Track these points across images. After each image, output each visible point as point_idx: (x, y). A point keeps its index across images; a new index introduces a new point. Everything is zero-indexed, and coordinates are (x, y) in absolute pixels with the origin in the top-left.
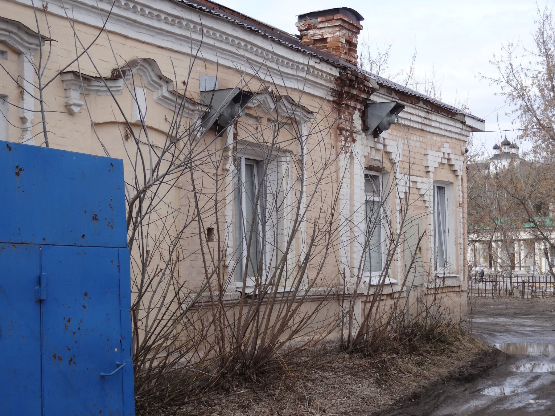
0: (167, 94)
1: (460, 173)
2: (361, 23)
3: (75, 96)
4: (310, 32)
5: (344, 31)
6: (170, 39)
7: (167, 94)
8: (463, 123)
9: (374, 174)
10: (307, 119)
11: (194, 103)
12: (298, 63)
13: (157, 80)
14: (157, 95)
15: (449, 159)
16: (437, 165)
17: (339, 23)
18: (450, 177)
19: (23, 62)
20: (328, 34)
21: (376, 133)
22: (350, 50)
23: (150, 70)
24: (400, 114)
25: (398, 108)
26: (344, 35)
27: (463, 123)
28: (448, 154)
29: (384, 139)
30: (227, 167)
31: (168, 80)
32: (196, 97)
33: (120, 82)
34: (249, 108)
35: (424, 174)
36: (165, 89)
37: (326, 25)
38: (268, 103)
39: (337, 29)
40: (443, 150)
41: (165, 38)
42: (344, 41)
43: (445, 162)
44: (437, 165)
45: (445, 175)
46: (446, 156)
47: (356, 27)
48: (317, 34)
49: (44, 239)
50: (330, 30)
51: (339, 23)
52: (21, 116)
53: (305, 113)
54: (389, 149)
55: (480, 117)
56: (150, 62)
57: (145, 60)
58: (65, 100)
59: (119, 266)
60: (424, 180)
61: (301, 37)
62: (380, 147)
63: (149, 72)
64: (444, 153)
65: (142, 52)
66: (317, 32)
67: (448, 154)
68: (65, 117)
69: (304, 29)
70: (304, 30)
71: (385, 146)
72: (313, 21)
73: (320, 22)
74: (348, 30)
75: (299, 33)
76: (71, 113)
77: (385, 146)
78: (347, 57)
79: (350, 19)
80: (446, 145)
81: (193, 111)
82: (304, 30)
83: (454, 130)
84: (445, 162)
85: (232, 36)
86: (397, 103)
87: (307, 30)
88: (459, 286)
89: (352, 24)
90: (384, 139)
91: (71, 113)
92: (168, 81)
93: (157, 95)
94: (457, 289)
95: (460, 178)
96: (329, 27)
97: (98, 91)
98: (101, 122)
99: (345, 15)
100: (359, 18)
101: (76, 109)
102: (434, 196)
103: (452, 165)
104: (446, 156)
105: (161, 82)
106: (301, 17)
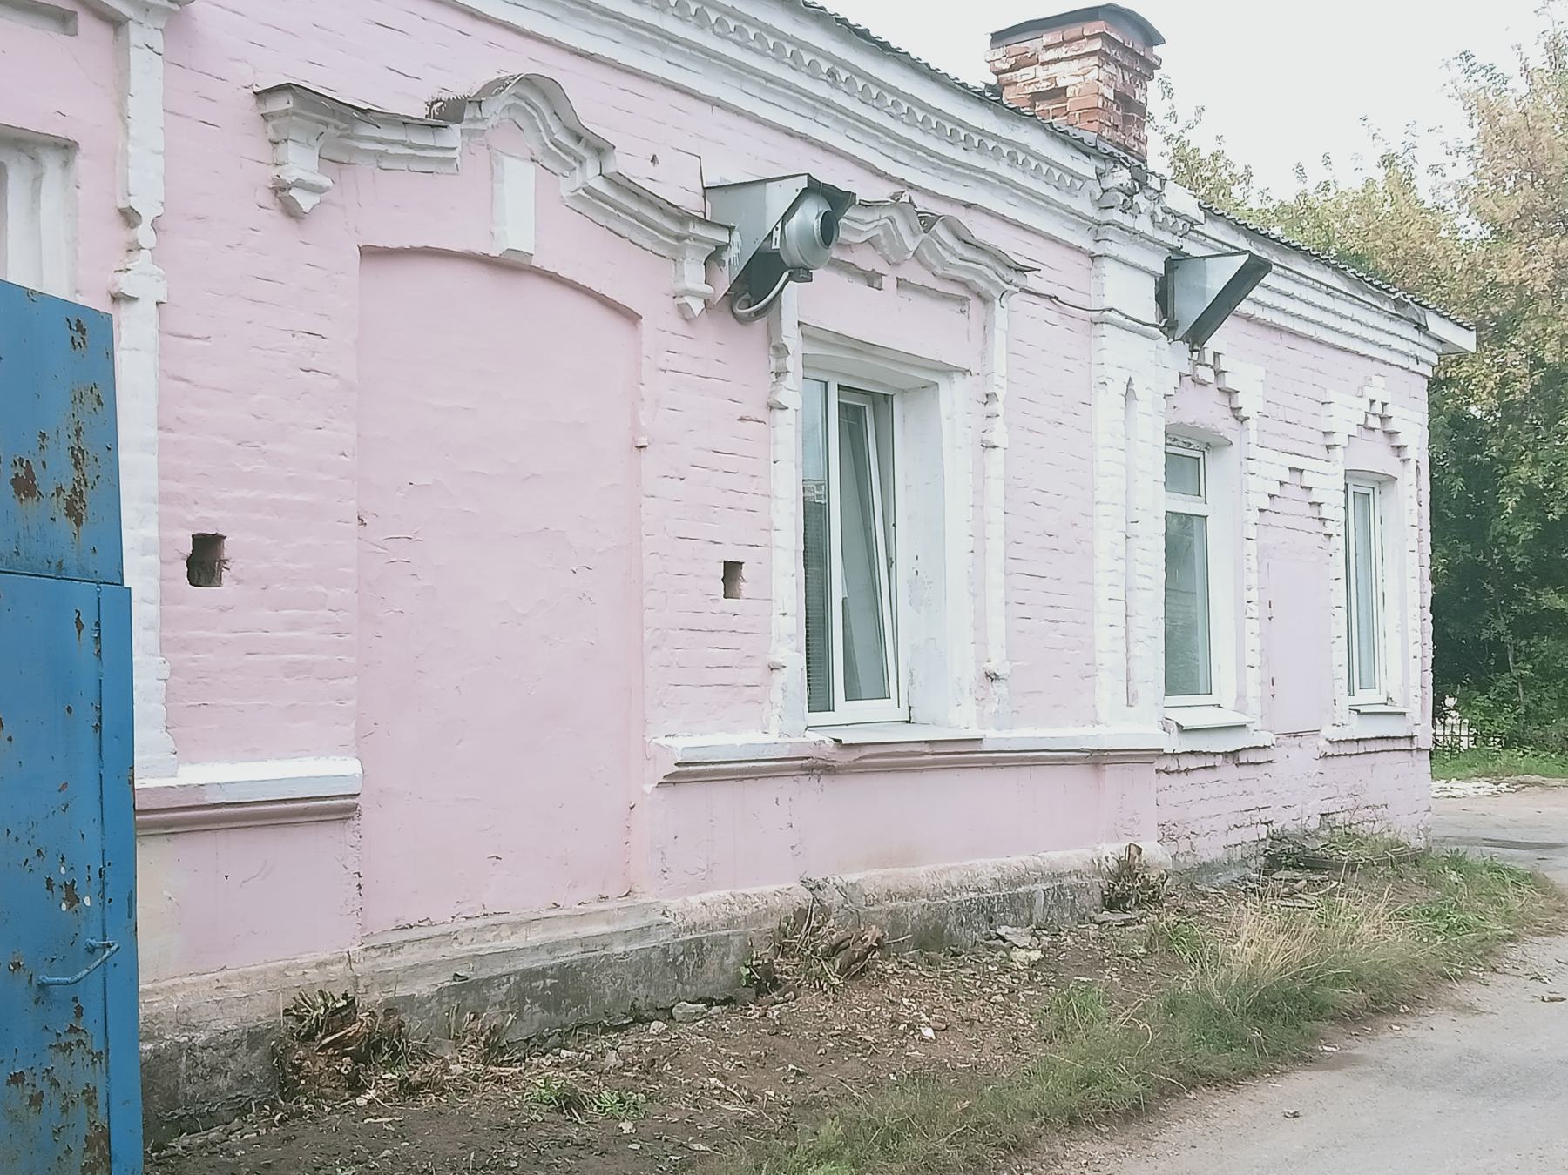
0: (600, 186)
1: (1411, 453)
2: (1157, 50)
3: (300, 163)
4: (1026, 73)
5: (1112, 69)
6: (607, 31)
7: (600, 186)
8: (1421, 328)
9: (1187, 455)
10: (1007, 287)
11: (683, 218)
12: (981, 132)
13: (570, 143)
14: (567, 186)
15: (1384, 419)
16: (1354, 431)
17: (1097, 45)
18: (1384, 462)
19: (126, 48)
20: (1066, 75)
21: (1197, 335)
22: (1127, 120)
23: (546, 112)
24: (1256, 293)
25: (1253, 272)
26: (1112, 77)
27: (1421, 328)
28: (1384, 404)
29: (1216, 355)
30: (783, 397)
31: (602, 145)
32: (691, 202)
33: (453, 136)
34: (848, 246)
35: (1322, 453)
36: (592, 168)
37: (1062, 52)
38: (899, 235)
39: (1094, 60)
40: (1370, 393)
41: (591, 29)
42: (1110, 95)
43: (1374, 422)
44: (1354, 431)
45: (1376, 457)
46: (1378, 408)
47: (1143, 59)
48: (1035, 77)
49: (204, 560)
50: (1075, 65)
51: (1097, 45)
52: (121, 206)
53: (1002, 271)
54: (1229, 382)
55: (692, 795)
56: (539, 88)
57: (527, 81)
58: (274, 172)
59: (98, 727)
60: (1322, 466)
61: (997, 90)
62: (1206, 374)
63: (543, 118)
64: (1372, 402)
65: (521, 60)
66: (1041, 72)
67: (1384, 404)
68: (273, 218)
69: (1007, 66)
70: (1005, 71)
71: (1219, 373)
72: (1032, 45)
73: (1047, 48)
74: (1123, 67)
75: (993, 80)
76: (292, 212)
77: (1219, 373)
78: (1119, 137)
79: (1133, 45)
80: (1377, 381)
81: (679, 238)
82: (1005, 71)
83: (1397, 344)
84: (1374, 422)
85: (791, 40)
86: (1252, 255)
87: (1013, 69)
88: (1412, 738)
89: (1131, 51)
90: (1216, 355)
91: (292, 212)
92: (601, 150)
93: (567, 186)
94: (1405, 745)
95: (1413, 464)
96: (1072, 58)
97: (382, 155)
98: (393, 244)
99: (1111, 24)
100: (1152, 38)
101: (305, 201)
102: (1346, 508)
103: (1392, 434)
104: (1378, 408)
105: (579, 149)
106: (998, 37)
